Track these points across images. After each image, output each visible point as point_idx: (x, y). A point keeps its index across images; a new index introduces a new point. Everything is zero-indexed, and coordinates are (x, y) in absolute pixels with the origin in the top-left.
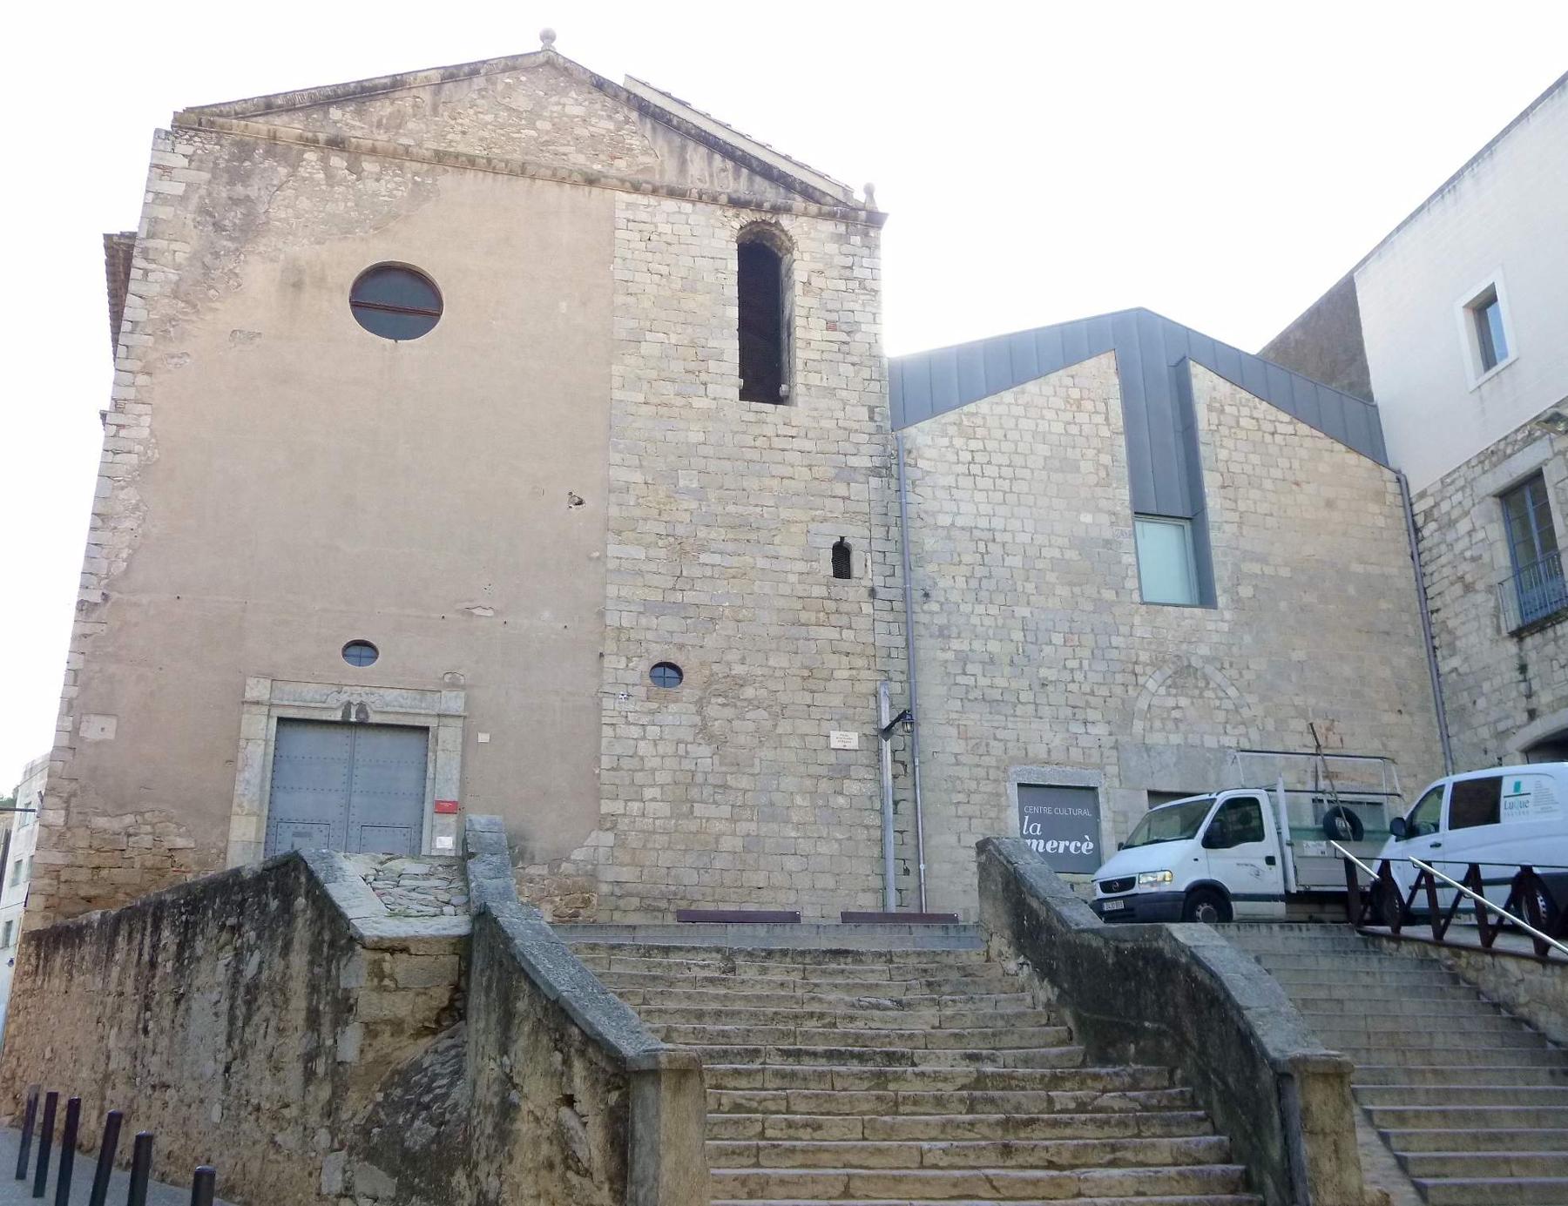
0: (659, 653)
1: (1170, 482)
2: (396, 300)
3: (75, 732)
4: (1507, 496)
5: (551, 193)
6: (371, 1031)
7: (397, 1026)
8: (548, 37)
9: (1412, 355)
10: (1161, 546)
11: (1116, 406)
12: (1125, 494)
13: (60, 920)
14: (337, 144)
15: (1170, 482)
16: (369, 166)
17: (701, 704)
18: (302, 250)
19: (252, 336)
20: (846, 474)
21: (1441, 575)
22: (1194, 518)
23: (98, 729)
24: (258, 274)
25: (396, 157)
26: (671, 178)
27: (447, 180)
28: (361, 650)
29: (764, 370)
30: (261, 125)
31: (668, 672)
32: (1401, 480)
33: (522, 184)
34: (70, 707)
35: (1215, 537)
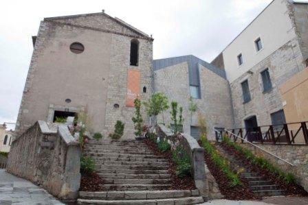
0: (115, 103)
1: (195, 81)
2: (77, 48)
3: (22, 111)
4: (242, 84)
5: (102, 33)
6: (43, 148)
7: (47, 148)
8: (103, 11)
9: (230, 65)
10: (193, 90)
11: (187, 69)
12: (188, 82)
13: (216, 190)
14: (69, 24)
15: (195, 81)
16: (74, 28)
17: (122, 110)
18: (63, 40)
19: (54, 52)
20: (146, 77)
21: (233, 94)
22: (198, 86)
23: (26, 111)
24: (55, 43)
25: (78, 27)
26: (120, 31)
27: (86, 31)
28: (68, 101)
29: (134, 61)
30: (58, 21)
31: (116, 106)
32: (228, 82)
33: (97, 32)
34: (21, 108)
35: (201, 89)
